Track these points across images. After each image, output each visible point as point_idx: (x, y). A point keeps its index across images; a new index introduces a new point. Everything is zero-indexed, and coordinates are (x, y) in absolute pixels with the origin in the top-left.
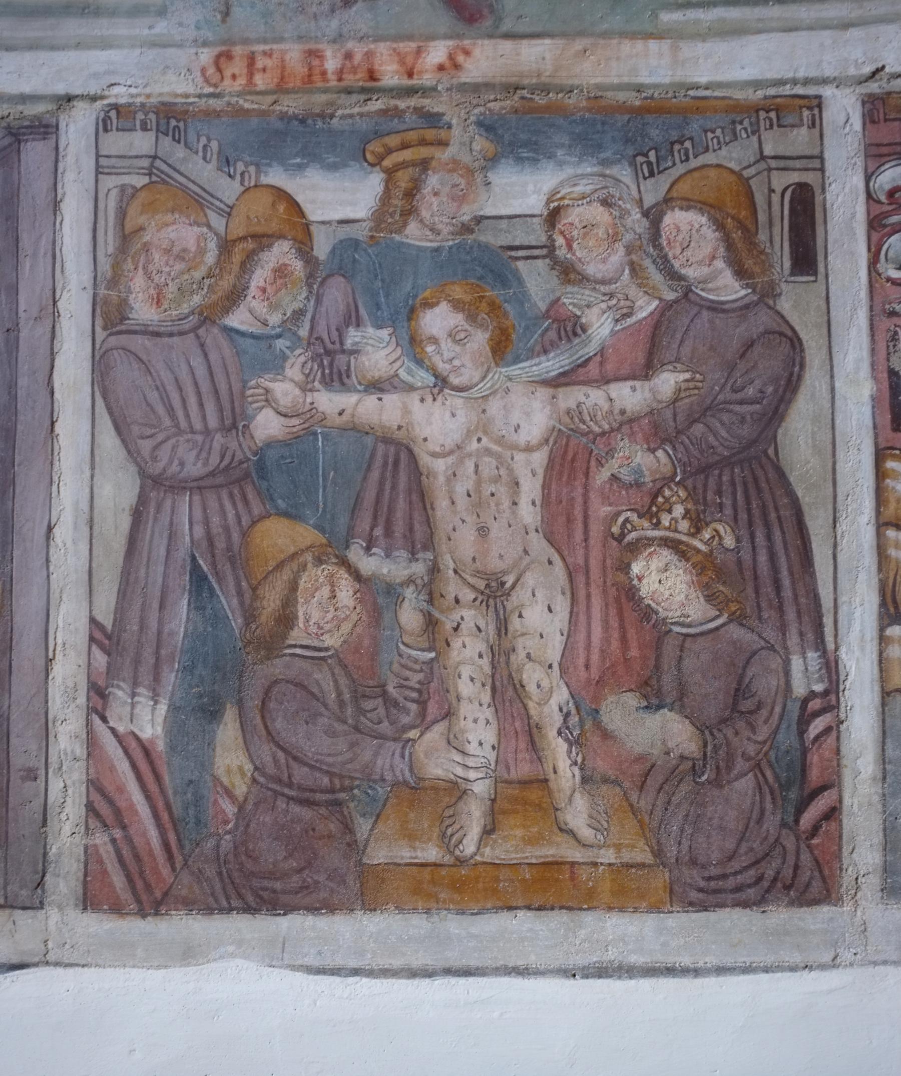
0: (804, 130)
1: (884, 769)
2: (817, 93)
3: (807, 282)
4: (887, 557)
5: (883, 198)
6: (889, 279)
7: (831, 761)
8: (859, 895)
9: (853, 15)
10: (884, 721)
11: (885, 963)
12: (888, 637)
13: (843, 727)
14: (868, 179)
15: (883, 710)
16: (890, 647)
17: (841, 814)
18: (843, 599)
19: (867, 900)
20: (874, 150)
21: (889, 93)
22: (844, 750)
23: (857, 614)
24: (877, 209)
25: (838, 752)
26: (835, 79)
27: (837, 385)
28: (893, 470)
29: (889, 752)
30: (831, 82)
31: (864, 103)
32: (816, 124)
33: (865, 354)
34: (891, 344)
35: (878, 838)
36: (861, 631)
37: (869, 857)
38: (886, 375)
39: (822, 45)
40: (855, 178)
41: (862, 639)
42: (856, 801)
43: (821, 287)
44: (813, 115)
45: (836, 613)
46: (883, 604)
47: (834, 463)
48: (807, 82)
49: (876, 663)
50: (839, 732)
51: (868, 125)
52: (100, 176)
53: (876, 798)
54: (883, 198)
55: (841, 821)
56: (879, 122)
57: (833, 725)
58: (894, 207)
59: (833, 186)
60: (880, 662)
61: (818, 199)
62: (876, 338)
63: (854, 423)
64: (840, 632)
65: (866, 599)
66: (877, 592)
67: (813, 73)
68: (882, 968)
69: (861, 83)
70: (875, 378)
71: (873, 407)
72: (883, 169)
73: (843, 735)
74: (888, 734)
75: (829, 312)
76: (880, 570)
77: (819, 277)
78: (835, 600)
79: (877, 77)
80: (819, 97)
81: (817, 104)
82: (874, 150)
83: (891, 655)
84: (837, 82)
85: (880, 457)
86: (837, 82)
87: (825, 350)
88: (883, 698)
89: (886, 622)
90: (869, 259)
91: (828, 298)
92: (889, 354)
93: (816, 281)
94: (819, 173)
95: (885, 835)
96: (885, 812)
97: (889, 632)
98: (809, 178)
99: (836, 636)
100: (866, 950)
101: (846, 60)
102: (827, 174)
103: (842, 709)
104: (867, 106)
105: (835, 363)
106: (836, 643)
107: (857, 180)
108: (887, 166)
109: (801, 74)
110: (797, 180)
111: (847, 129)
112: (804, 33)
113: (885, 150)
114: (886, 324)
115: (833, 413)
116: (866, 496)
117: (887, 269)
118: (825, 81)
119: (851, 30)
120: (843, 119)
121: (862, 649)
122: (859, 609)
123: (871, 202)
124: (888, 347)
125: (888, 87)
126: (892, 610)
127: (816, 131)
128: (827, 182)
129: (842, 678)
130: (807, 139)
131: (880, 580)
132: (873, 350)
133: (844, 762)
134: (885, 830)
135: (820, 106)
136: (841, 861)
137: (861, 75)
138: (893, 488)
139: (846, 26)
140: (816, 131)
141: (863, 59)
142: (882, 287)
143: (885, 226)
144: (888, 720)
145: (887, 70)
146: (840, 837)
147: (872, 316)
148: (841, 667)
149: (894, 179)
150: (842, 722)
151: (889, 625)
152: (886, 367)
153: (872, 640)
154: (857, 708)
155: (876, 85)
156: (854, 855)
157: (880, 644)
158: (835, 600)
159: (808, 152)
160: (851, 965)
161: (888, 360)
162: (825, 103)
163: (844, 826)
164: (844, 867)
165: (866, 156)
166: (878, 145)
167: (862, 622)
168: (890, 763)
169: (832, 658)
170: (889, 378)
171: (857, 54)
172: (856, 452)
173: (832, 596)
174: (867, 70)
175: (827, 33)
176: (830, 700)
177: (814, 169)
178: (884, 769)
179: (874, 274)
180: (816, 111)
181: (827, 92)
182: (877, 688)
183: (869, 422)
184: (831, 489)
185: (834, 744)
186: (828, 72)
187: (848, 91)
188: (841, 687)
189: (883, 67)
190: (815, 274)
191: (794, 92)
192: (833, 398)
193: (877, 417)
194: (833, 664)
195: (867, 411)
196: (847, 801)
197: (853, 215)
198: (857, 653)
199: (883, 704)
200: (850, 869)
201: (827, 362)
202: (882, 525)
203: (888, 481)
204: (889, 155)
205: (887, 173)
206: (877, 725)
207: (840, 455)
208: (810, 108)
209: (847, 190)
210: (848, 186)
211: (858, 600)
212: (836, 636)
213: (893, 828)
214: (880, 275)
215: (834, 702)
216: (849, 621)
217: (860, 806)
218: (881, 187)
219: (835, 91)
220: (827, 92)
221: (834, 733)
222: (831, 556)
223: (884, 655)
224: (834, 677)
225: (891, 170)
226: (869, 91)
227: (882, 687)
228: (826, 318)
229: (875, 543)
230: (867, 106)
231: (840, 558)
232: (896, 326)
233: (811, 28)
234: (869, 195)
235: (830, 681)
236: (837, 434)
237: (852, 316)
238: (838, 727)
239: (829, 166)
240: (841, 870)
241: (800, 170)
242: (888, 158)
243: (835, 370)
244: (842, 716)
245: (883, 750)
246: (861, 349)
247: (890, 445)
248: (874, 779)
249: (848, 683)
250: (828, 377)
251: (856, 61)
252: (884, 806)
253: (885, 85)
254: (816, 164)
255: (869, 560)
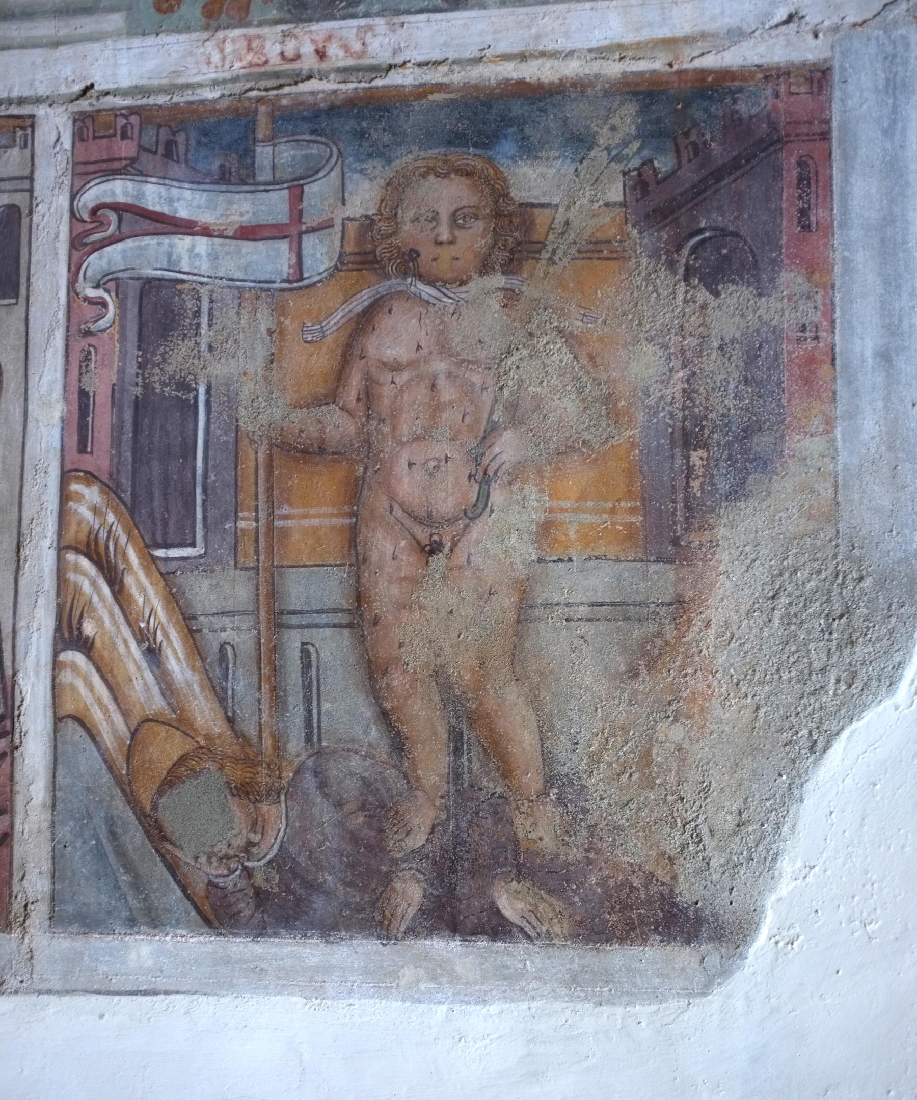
0: (15, 151)
1: (54, 796)
2: (31, 113)
3: (9, 305)
4: (66, 581)
5: (86, 217)
6: (86, 299)
7: (5, 787)
8: (28, 922)
9: (61, 33)
10: (55, 747)
11: (49, 992)
12: (61, 663)
13: (16, 754)
14: (73, 197)
15: (55, 736)
16: (63, 673)
17: (12, 840)
18: (21, 624)
19: (35, 928)
20: (81, 169)
21: (99, 111)
22: (18, 776)
23: (34, 639)
24: (80, 228)
25: (12, 778)
26: (48, 97)
27: (30, 407)
28: (77, 493)
29: (59, 778)
30: (44, 101)
31: (75, 121)
32: (28, 144)
33: (59, 375)
34: (84, 364)
35: (46, 866)
36: (37, 656)
37: (39, 884)
38: (76, 396)
39: (33, 63)
40: (61, 197)
41: (37, 664)
42: (26, 827)
43: (20, 310)
44: (26, 136)
45: (14, 638)
46: (58, 629)
47: (22, 487)
48: (21, 101)
49: (49, 688)
50: (13, 759)
51: (77, 144)
52: (26, 173)
53: (46, 825)
54: (86, 217)
55: (12, 847)
56: (87, 141)
57: (8, 751)
58: (94, 225)
59: (40, 206)
60: (53, 687)
61: (25, 221)
62: (70, 359)
63: (43, 445)
64: (17, 657)
65: (43, 623)
66: (54, 617)
67: (27, 93)
68: (46, 996)
69: (72, 101)
70: (66, 399)
71: (63, 429)
72: (88, 186)
73: (18, 761)
74: (60, 760)
75: (27, 335)
76: (58, 594)
77: (20, 299)
78: (14, 625)
79: (88, 95)
80: (32, 116)
81: (28, 124)
82: (81, 169)
83: (64, 680)
84: (49, 101)
85: (65, 478)
86: (49, 101)
87: (21, 372)
88: (55, 724)
89: (59, 647)
90: (68, 279)
91: (27, 320)
92: (81, 374)
93: (16, 304)
94: (27, 194)
95: (54, 863)
96: (53, 840)
97: (62, 657)
98: (19, 199)
99: (14, 661)
100: (31, 978)
101: (57, 78)
102: (35, 194)
103: (17, 736)
104: (78, 124)
105: (30, 386)
106: (13, 668)
107: (63, 200)
108: (92, 184)
109: (15, 94)
110: (6, 202)
111: (57, 149)
112: (16, 52)
113: (91, 168)
114: (81, 344)
115: (24, 436)
116: (50, 519)
117: (84, 288)
118: (38, 100)
119: (61, 48)
120: (53, 138)
121: (37, 675)
122: (35, 634)
123: (74, 220)
124: (81, 367)
125: (98, 105)
126: (66, 634)
127: (27, 152)
128: (34, 203)
129: (17, 703)
130: (18, 160)
131: (58, 605)
132: (66, 371)
133: (17, 788)
134: (53, 858)
135: (32, 126)
136: (11, 887)
137: (72, 94)
138: (76, 511)
139: (56, 44)
140: (27, 152)
141: (73, 78)
142: (79, 306)
143: (86, 244)
144: (59, 746)
145: (96, 87)
146: (11, 863)
147: (68, 336)
148: (17, 692)
149: (97, 197)
150: (17, 748)
151: (63, 650)
152: (77, 388)
153: (46, 665)
154: (31, 734)
155: (86, 103)
156: (25, 882)
157: (54, 669)
158: (14, 625)
159: (18, 173)
160: (16, 992)
161: (80, 381)
162: (38, 122)
163: (15, 853)
164: (14, 894)
165: (74, 175)
166: (86, 163)
167: (38, 647)
168: (59, 790)
169: (9, 684)
170: (80, 398)
171: (67, 71)
172: (42, 475)
173: (11, 621)
174: (77, 88)
175: (37, 51)
176: (5, 726)
177: (22, 190)
178: (54, 796)
179: (72, 294)
180: (29, 131)
181: (41, 111)
182: (50, 714)
183: (57, 444)
184: (17, 514)
185: (8, 771)
186: (42, 90)
187: (61, 109)
188: (16, 713)
189: (92, 86)
190: (17, 296)
191: (9, 112)
192: (25, 421)
193: (66, 440)
194: (9, 689)
195: (56, 433)
196: (18, 827)
197: (57, 236)
198: (32, 679)
199: (56, 730)
200: (20, 896)
201: (23, 385)
202: (62, 548)
203: (71, 503)
204: (95, 173)
205: (92, 191)
206: (49, 751)
207: (28, 476)
208: (23, 128)
209: (52, 210)
210: (54, 205)
211: (35, 625)
212: (14, 661)
213: (62, 856)
214: (77, 294)
215: (8, 728)
216: (27, 646)
217: (30, 832)
218: (85, 205)
219: (49, 110)
220: (41, 111)
221: (8, 759)
222: (12, 581)
223: (57, 680)
224: (10, 703)
225: (95, 188)
226: (80, 109)
227: (55, 713)
228: (24, 341)
229: (55, 567)
230: (78, 124)
231: (22, 582)
232: (90, 345)
233: (23, 47)
234: (73, 214)
235: (6, 706)
236: (26, 457)
237: (49, 337)
238: (12, 753)
239: (37, 186)
240: (10, 897)
241: (10, 191)
242: (93, 176)
243: (30, 392)
244: (17, 741)
245: (54, 777)
246: (55, 370)
247: (75, 467)
248: (44, 806)
249: (23, 709)
250: (22, 399)
251: (67, 79)
252: (53, 833)
253: (95, 103)
254: (26, 185)
255: (49, 583)
